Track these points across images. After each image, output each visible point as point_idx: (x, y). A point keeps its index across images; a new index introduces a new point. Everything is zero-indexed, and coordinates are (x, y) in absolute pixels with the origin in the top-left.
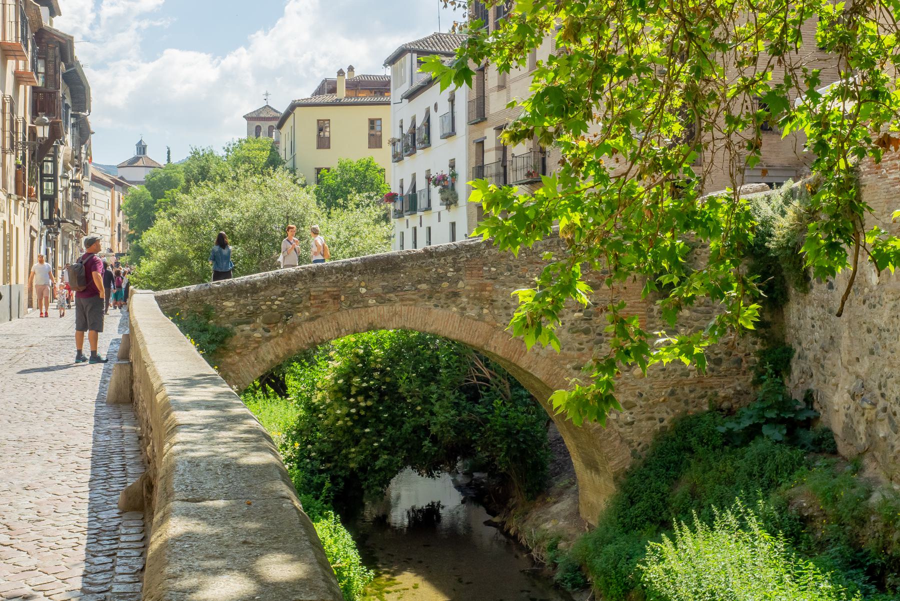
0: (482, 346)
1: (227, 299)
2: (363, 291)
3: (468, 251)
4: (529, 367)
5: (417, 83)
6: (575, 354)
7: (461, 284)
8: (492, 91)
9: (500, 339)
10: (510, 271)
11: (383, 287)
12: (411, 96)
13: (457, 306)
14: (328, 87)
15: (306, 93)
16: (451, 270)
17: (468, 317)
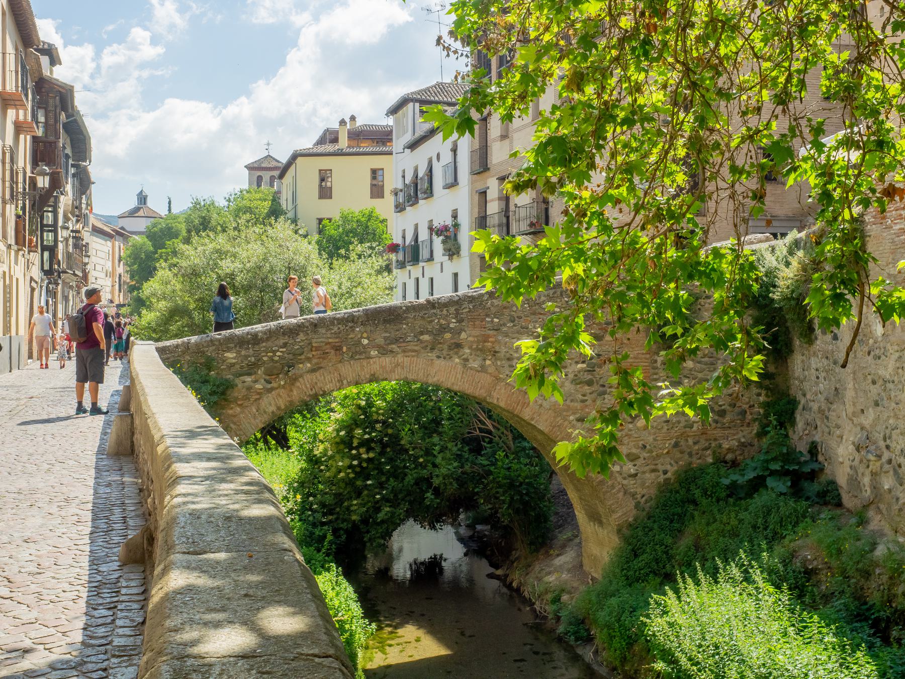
0: (485, 398)
1: (229, 350)
2: (365, 342)
3: (471, 302)
4: (532, 419)
5: (419, 133)
6: (578, 405)
7: (463, 335)
8: (494, 140)
9: (503, 391)
10: (513, 322)
11: (385, 338)
12: (413, 146)
13: (459, 357)
14: (330, 137)
15: (307, 143)
16: (454, 320)
17: (471, 368)
